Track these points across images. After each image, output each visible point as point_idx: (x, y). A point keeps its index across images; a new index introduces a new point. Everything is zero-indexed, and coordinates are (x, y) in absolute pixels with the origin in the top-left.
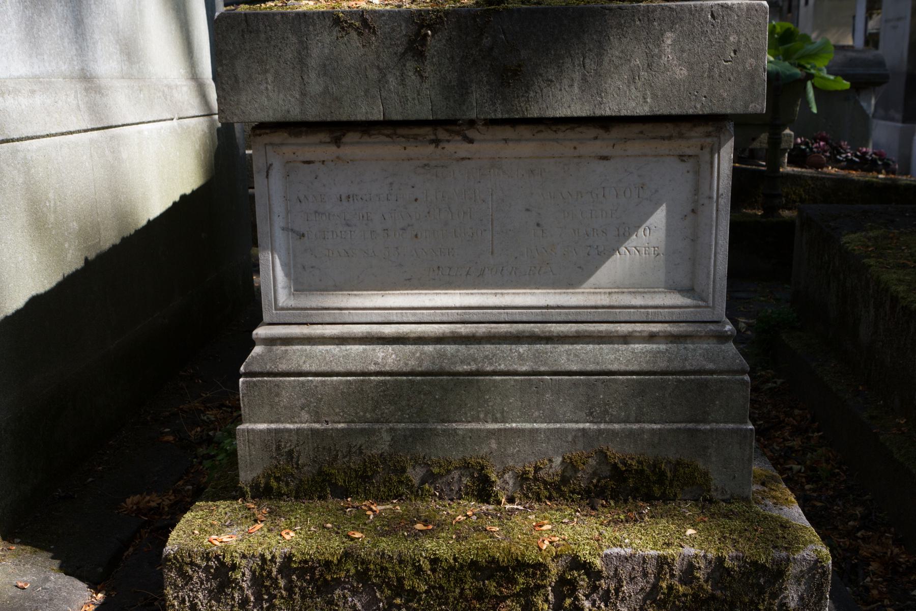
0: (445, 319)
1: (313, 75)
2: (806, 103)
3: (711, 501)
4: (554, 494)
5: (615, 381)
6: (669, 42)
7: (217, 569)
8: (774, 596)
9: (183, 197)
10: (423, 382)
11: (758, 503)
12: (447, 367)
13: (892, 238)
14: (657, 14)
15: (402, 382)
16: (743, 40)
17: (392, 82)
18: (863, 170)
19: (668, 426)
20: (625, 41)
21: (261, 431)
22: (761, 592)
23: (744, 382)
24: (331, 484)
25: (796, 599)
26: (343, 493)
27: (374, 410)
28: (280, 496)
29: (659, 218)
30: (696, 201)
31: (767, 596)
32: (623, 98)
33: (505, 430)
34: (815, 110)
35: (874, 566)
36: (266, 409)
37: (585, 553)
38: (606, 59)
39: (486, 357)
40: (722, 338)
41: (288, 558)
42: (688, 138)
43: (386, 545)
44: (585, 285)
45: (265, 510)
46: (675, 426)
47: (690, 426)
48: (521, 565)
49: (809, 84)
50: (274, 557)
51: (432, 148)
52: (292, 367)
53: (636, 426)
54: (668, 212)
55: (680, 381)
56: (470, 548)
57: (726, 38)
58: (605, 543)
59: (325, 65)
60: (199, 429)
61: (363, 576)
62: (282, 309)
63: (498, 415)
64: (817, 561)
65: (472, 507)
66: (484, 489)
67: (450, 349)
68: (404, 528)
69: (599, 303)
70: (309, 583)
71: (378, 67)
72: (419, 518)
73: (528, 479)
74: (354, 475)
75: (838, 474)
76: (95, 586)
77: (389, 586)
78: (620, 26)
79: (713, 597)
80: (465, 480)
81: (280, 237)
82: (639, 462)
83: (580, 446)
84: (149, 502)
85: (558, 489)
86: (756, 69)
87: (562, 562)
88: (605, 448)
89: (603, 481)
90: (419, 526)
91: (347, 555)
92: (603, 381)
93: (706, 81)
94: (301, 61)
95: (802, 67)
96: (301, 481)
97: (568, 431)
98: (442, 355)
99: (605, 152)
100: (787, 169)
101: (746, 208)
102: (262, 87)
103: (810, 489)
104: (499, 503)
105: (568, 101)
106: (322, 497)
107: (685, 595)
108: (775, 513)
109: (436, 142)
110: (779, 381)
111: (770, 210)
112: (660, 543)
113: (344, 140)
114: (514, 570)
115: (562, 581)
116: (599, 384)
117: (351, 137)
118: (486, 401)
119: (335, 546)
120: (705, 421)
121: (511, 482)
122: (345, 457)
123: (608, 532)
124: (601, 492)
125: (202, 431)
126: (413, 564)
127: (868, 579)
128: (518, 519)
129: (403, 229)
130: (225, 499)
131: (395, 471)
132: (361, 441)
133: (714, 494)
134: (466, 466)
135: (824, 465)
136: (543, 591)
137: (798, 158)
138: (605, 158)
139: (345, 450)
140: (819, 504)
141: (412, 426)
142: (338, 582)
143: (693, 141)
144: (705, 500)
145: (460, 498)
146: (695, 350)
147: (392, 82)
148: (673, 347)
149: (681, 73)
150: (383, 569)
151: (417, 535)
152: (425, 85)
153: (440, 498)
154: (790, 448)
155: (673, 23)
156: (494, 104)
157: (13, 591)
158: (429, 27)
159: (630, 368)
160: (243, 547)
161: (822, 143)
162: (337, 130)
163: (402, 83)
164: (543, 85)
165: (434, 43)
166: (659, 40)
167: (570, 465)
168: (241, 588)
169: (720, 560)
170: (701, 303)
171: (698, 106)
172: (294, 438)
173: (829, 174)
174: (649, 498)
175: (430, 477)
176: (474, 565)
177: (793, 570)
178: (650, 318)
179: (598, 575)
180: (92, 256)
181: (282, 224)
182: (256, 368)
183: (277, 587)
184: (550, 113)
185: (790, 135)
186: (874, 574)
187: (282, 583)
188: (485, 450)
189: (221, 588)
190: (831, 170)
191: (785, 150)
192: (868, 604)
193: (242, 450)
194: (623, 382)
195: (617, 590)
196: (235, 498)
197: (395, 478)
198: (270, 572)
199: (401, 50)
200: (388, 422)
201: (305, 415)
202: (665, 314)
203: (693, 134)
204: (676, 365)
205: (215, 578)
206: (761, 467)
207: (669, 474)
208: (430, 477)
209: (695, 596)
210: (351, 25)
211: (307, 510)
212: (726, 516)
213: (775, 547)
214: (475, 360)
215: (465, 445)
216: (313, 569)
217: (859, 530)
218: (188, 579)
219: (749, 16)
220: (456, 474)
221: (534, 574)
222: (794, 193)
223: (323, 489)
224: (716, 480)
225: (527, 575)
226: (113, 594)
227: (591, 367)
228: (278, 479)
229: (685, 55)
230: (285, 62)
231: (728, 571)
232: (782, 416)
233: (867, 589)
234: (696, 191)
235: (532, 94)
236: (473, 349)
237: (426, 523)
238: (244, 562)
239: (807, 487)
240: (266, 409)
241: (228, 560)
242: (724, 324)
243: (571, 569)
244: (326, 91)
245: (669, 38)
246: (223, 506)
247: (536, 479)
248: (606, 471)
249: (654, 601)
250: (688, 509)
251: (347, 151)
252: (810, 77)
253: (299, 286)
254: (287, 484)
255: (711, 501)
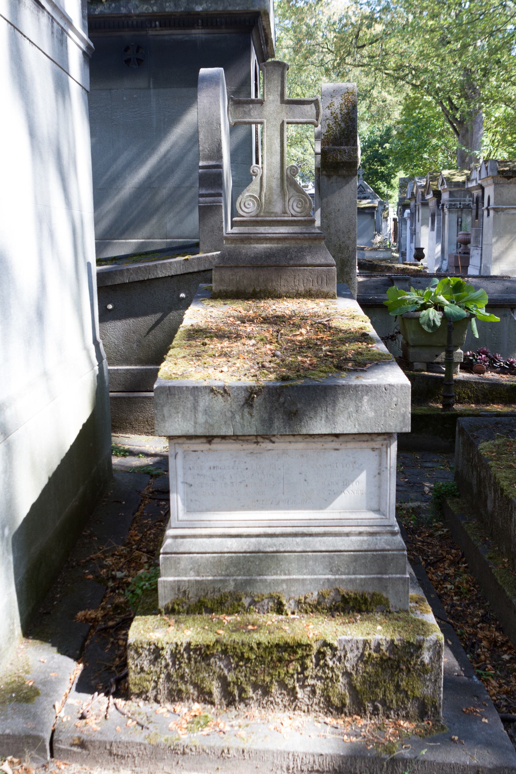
0: (261, 525)
1: (200, 414)
2: (471, 332)
3: (390, 612)
4: (314, 610)
5: (343, 555)
6: (366, 400)
7: (154, 650)
8: (418, 657)
9: (84, 425)
10: (250, 557)
11: (412, 612)
12: (262, 549)
13: (508, 446)
14: (360, 388)
15: (240, 557)
16: (399, 400)
17: (238, 418)
18: (511, 374)
19: (368, 576)
20: (345, 400)
21: (170, 581)
22: (412, 655)
23: (404, 555)
24: (204, 607)
25: (428, 658)
26: (210, 611)
27: (226, 570)
28: (179, 613)
29: (363, 477)
30: (380, 469)
31: (414, 658)
32: (345, 425)
33: (290, 579)
34: (477, 336)
35: (484, 643)
36: (173, 570)
37: (329, 640)
38: (337, 408)
39: (281, 544)
40: (394, 534)
41: (189, 644)
42: (375, 441)
43: (236, 637)
44: (328, 508)
45: (173, 621)
46: (372, 576)
47: (379, 576)
48: (300, 645)
49: (473, 320)
50: (182, 643)
51: (255, 445)
52: (186, 550)
53: (353, 577)
54: (367, 474)
55: (373, 555)
56: (276, 638)
57: (392, 399)
58: (339, 633)
59: (206, 410)
60: (105, 570)
61: (225, 652)
62: (181, 521)
63: (287, 572)
64: (437, 641)
65: (274, 617)
66: (280, 608)
67: (263, 540)
68: (243, 628)
69: (335, 517)
70: (199, 655)
71: (231, 411)
72: (249, 623)
73: (301, 603)
74: (216, 602)
75: (473, 590)
76: (77, 659)
77: (237, 656)
78: (343, 393)
79: (390, 659)
80: (271, 604)
81: (180, 486)
82: (355, 594)
83: (326, 586)
84: (90, 615)
85: (316, 607)
86: (405, 413)
87: (319, 643)
88: (338, 587)
89: (338, 604)
90: (250, 627)
91: (217, 641)
92: (337, 555)
93: (383, 418)
94: (195, 408)
95: (467, 309)
96: (190, 605)
97: (320, 579)
98: (259, 543)
99: (337, 447)
100: (460, 375)
101: (432, 403)
102: (176, 420)
103: (456, 600)
104: (287, 615)
105: (319, 426)
106: (200, 613)
107: (376, 658)
108: (420, 618)
109: (257, 443)
110: (445, 530)
111: (447, 406)
112: (365, 633)
113: (213, 441)
114: (296, 647)
115: (319, 652)
116: (335, 557)
117: (216, 440)
118: (281, 565)
119: (210, 638)
120: (386, 573)
121: (293, 604)
122: (211, 593)
123: (341, 628)
124: (337, 609)
125: (107, 571)
126: (249, 646)
127: (480, 650)
128: (297, 623)
129: (241, 482)
130: (151, 614)
131: (236, 600)
132: (220, 585)
133: (391, 609)
134: (271, 597)
135: (465, 585)
136: (310, 657)
137: (467, 366)
138: (337, 450)
139: (212, 590)
140: (459, 608)
141: (245, 578)
142: (213, 655)
143: (377, 444)
144: (387, 611)
145: (268, 612)
146: (381, 539)
147: (238, 418)
148: (370, 538)
149: (371, 414)
150: (234, 648)
151: (249, 631)
152: (253, 419)
153: (258, 612)
154: (448, 574)
155: (367, 392)
156: (285, 428)
157: (39, 664)
158: (255, 393)
159: (350, 549)
160: (166, 639)
161: (483, 356)
162: (210, 439)
163: (242, 418)
164: (308, 419)
165: (257, 400)
166: (361, 399)
167: (322, 596)
168: (166, 659)
169: (392, 641)
170: (383, 517)
171: (380, 429)
172: (187, 584)
173: (488, 379)
174: (360, 611)
175: (254, 603)
176: (277, 645)
177: (426, 645)
178: (359, 524)
179: (336, 649)
180: (50, 474)
181: (182, 480)
182: (168, 550)
183: (183, 658)
184: (311, 432)
185: (461, 353)
186: (484, 647)
187: (185, 656)
188: (280, 589)
189: (156, 659)
190: (489, 375)
191: (458, 363)
192: (477, 663)
193: (161, 590)
194: (347, 556)
195: (345, 656)
196: (156, 614)
197: (236, 603)
198: (180, 651)
199: (242, 403)
200: (233, 576)
201: (192, 573)
202: (366, 522)
203: (378, 439)
204: (372, 547)
205: (153, 653)
206: (415, 593)
207: (369, 600)
208: (254, 603)
209: (381, 658)
210: (218, 392)
211: (194, 620)
212: (396, 619)
213: (418, 634)
214: (275, 545)
215: (270, 587)
216: (200, 649)
217: (479, 623)
218: (140, 655)
219: (402, 389)
220: (266, 601)
221: (306, 649)
222: (464, 393)
223: (201, 609)
224: (392, 602)
225: (302, 649)
226: (87, 665)
227: (331, 549)
228: (178, 605)
229: (373, 406)
230: (187, 408)
231: (396, 646)
232: (444, 554)
233: (479, 655)
234: (380, 464)
235: (303, 424)
236: (275, 540)
237: (253, 625)
238: (168, 646)
239: (455, 598)
240: (173, 570)
241: (160, 646)
242: (395, 526)
243: (323, 646)
244: (206, 422)
245: (366, 399)
246: (151, 618)
247: (305, 603)
248: (339, 598)
249: (362, 661)
250: (379, 617)
251: (214, 446)
252: (473, 316)
253: (189, 510)
254: (183, 607)
255: (390, 612)
